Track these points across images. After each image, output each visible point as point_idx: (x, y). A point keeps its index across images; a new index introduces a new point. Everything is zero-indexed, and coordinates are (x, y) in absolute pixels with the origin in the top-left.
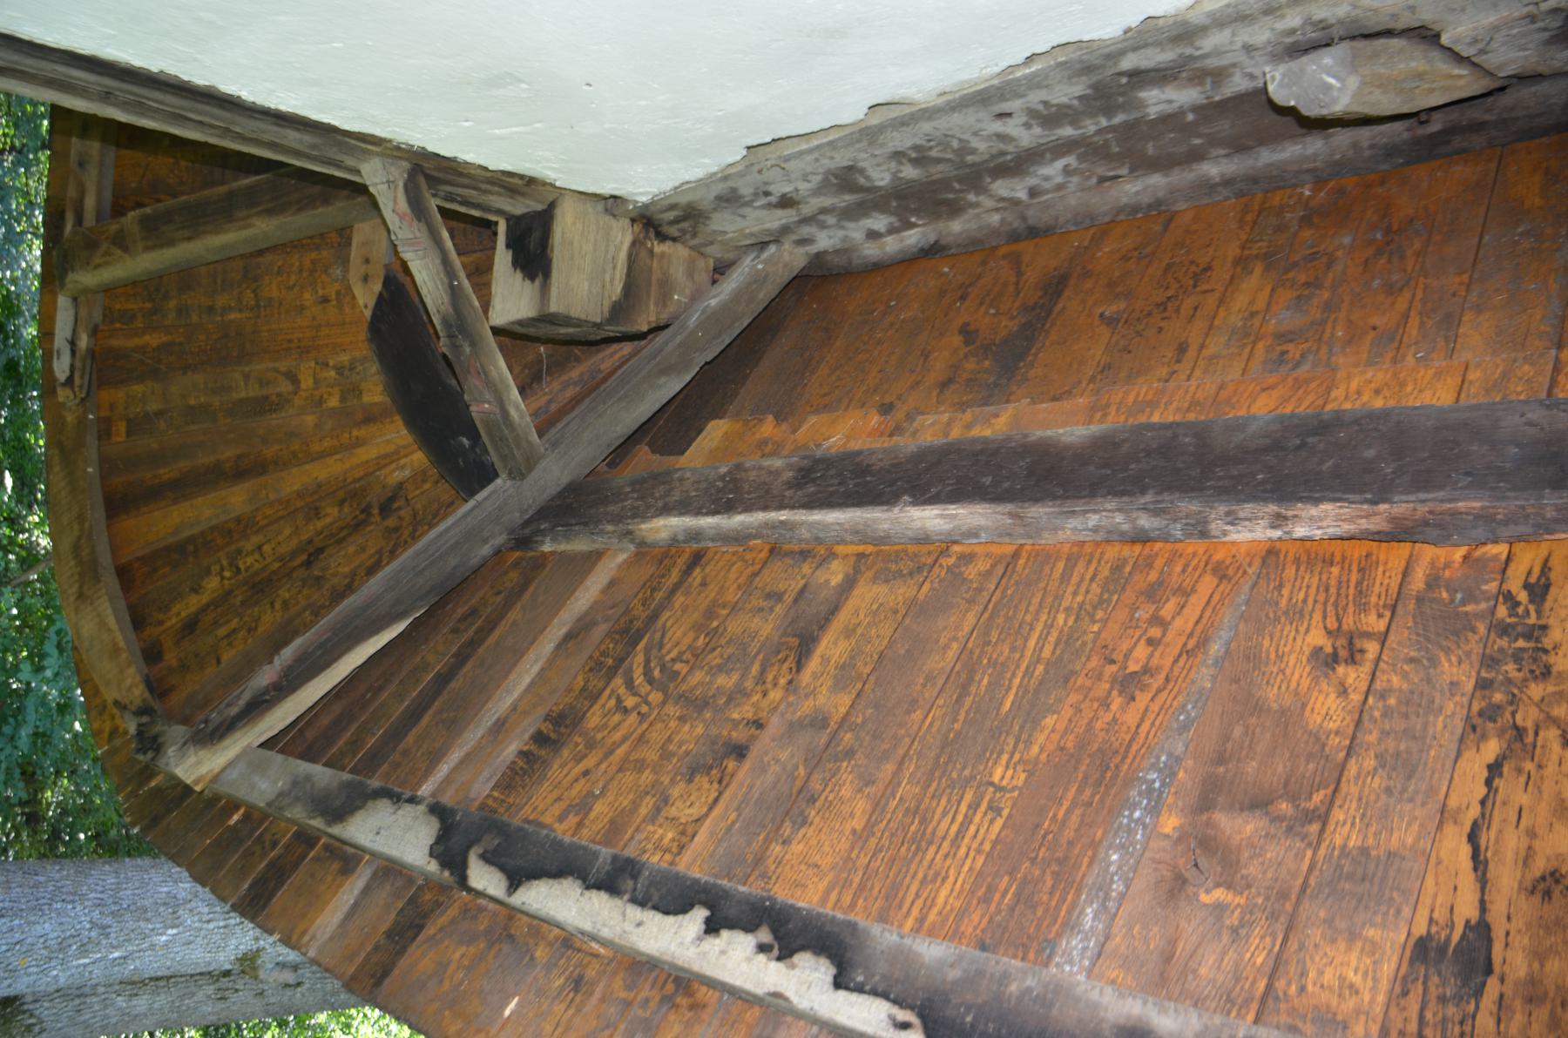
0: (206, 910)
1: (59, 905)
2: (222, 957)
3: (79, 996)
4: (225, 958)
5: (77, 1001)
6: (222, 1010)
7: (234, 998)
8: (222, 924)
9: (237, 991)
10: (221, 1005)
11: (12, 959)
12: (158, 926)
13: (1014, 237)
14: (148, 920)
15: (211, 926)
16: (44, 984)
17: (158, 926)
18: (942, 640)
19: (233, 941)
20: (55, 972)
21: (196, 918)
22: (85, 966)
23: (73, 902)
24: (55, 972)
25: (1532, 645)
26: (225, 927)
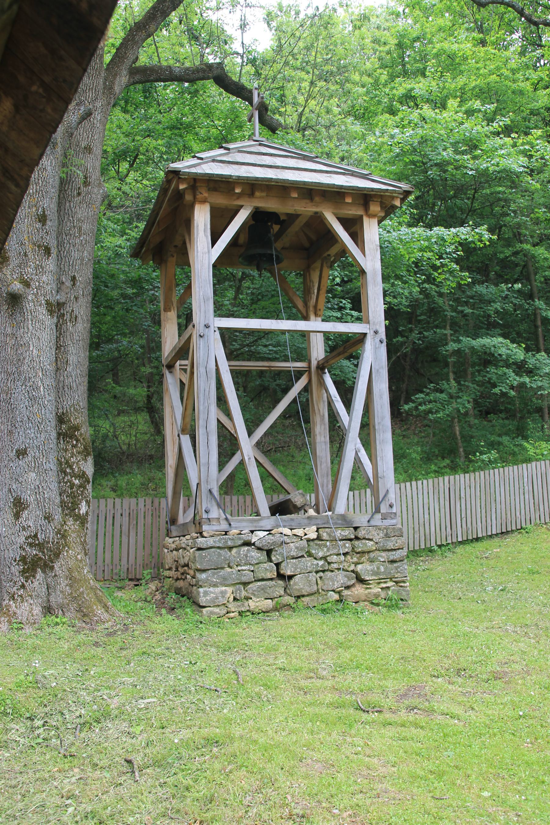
0: (22, 330)
1: (12, 400)
2: (48, 323)
3: (63, 389)
4: (49, 321)
5: (66, 389)
6: (82, 319)
7: (76, 312)
8: (30, 322)
9: (73, 311)
10: (79, 319)
11: (36, 421)
12: (28, 354)
13: (455, 143)
14: (24, 359)
15: (31, 328)
16: (51, 407)
17: (28, 354)
18: (485, 456)
19: (40, 317)
20: (46, 402)
21: (26, 335)
22: (44, 388)
23: (11, 394)
24: (46, 402)
25: (235, 765)
26: (32, 321)
